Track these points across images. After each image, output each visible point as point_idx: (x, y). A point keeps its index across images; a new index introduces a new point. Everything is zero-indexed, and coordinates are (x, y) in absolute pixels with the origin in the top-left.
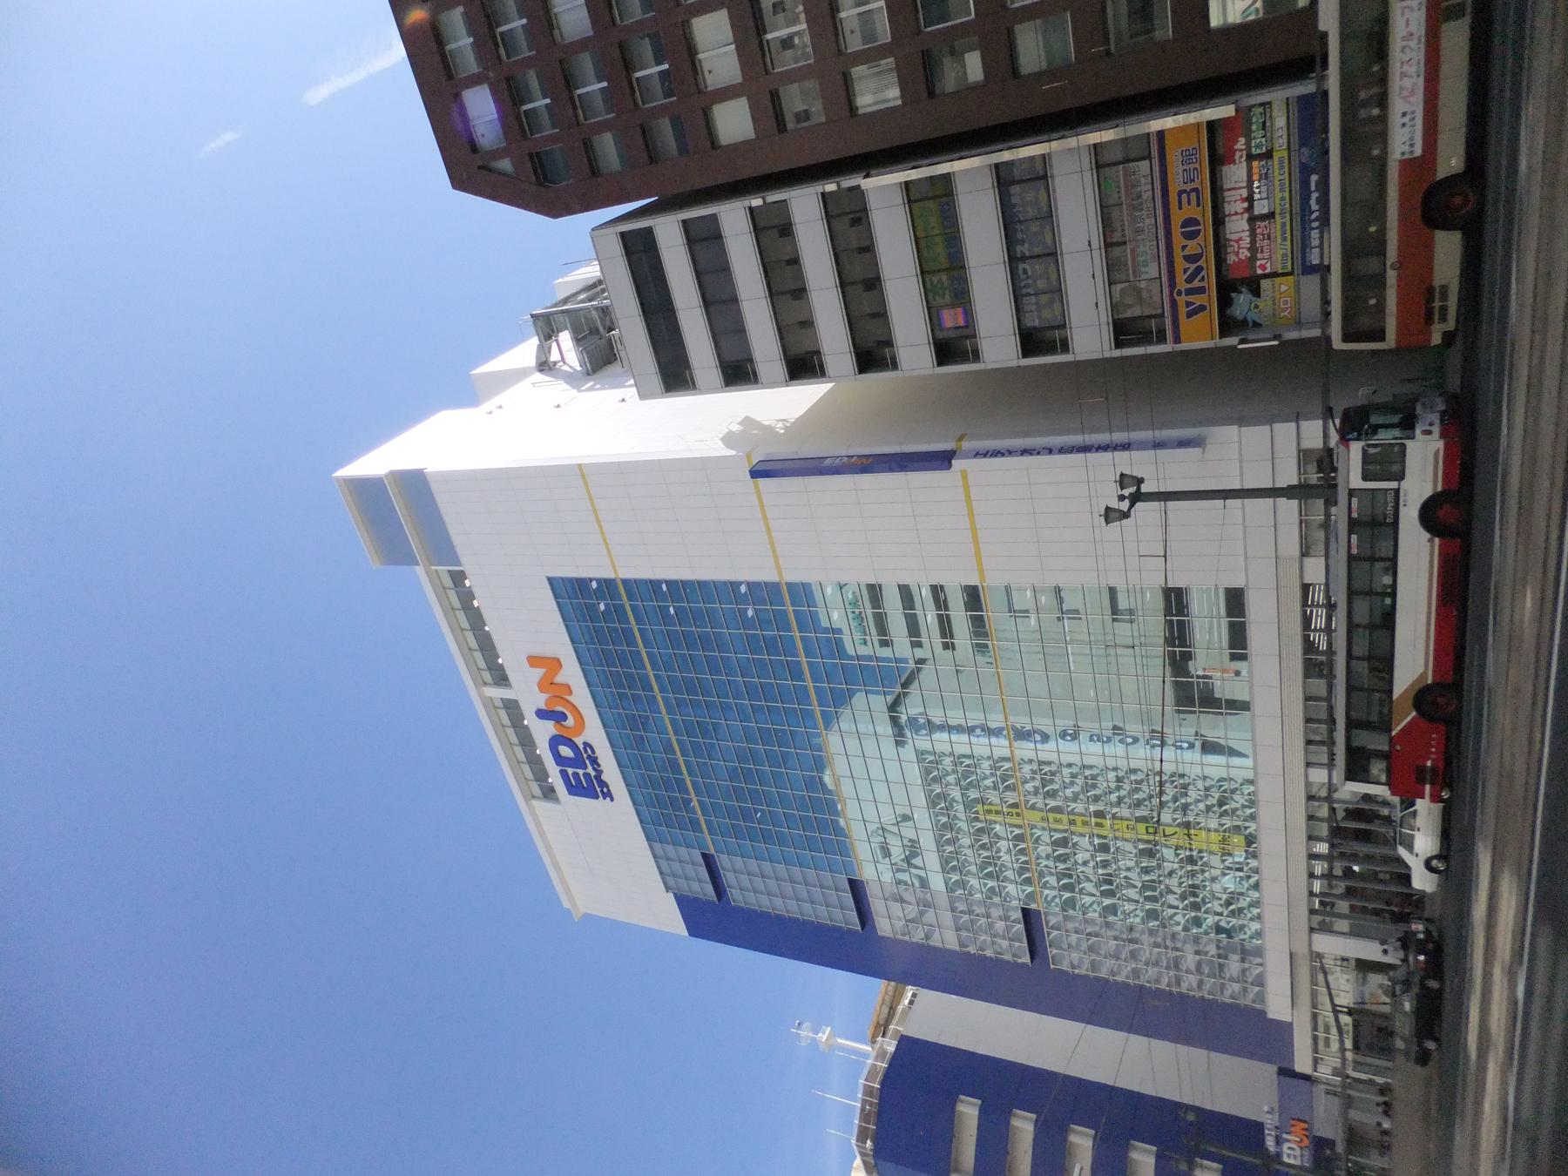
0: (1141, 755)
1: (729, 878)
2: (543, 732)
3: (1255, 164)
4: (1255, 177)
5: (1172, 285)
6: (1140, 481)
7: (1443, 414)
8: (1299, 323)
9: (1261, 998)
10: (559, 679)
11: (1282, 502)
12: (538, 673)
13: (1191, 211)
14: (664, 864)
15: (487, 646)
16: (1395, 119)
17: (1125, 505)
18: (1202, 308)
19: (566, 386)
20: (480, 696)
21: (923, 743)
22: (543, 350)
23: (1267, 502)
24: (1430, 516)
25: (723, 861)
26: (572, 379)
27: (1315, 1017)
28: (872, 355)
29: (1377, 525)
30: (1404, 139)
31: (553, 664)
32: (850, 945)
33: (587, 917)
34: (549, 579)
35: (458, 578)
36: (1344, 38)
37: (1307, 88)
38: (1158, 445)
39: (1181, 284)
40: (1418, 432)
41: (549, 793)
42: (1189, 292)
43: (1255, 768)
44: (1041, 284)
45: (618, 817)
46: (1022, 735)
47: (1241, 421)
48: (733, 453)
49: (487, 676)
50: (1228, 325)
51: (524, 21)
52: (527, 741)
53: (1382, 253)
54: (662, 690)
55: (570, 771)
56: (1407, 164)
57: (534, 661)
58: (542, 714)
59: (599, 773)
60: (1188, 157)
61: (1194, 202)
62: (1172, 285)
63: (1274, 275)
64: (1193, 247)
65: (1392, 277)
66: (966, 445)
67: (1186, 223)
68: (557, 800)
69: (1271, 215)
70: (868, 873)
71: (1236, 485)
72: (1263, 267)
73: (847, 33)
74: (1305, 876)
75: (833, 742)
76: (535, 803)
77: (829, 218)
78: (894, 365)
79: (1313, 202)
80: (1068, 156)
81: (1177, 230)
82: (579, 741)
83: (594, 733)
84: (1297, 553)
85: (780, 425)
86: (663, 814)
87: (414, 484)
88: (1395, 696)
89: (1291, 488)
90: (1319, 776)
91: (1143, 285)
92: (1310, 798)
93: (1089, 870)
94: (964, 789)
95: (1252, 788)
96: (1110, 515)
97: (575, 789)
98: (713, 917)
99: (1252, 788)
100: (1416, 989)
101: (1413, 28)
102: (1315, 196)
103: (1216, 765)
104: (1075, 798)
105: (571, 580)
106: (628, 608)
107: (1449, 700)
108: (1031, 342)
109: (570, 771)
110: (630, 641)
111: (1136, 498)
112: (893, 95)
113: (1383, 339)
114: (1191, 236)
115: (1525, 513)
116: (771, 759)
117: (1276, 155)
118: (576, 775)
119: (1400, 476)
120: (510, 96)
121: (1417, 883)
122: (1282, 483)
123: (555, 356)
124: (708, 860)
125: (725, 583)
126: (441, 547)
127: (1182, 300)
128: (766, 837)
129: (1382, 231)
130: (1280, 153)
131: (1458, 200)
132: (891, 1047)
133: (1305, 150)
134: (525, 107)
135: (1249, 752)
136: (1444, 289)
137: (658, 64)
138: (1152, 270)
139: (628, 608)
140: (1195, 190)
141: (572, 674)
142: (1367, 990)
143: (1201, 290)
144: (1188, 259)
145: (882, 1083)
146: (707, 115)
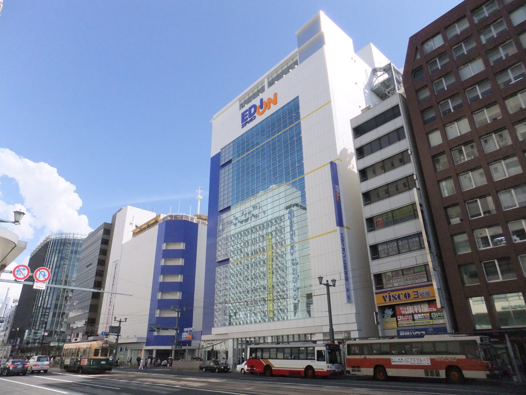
0: (291, 285)
1: (226, 168)
2: (256, 102)
3: (428, 314)
4: (425, 315)
5: (392, 291)
6: (334, 286)
7: (334, 371)
8: (384, 330)
9: (218, 326)
10: (272, 105)
11: (329, 327)
12: (272, 97)
13: (412, 296)
14: (224, 150)
15: (279, 77)
16: (400, 357)
17: (324, 282)
18: (385, 300)
19: (366, 82)
20: (264, 78)
21: (287, 217)
22: (380, 69)
23: (328, 323)
24: (309, 367)
25: (230, 166)
26: (370, 82)
27: (214, 340)
28: (368, 197)
29: (308, 354)
30: (396, 360)
31: (275, 103)
32: (216, 209)
33: (211, 124)
34: (298, 97)
35: (296, 63)
36: (421, 342)
37: (449, 329)
38: (348, 290)
39: (392, 294)
40: (329, 364)
41: (242, 106)
42: (390, 296)
43: (291, 320)
44: (390, 250)
45: (237, 130)
46: (292, 247)
47: (357, 314)
48: (338, 154)
49: (270, 79)
50: (383, 308)
51: (466, 53)
52: (255, 96)
53: (369, 354)
54: (278, 136)
55: (248, 113)
56: (389, 360)
57: (275, 95)
58: (262, 100)
59: (248, 122)
60: (428, 294)
61: (415, 296)
62: (392, 291)
63: (397, 321)
64: (402, 297)
65: (363, 357)
66: (345, 230)
67: (408, 293)
68: (240, 109)
69: (414, 320)
70: (233, 211)
71: (332, 314)
72: (399, 318)
73: (465, 176)
74: (311, 332)
75: (282, 188)
76: (238, 102)
77: (407, 177)
78: (365, 205)
79: (417, 332)
80: (425, 256)
81: (407, 291)
82: (256, 114)
83: (259, 119)
84: (324, 331)
85: (351, 166)
86: (241, 144)
87: (320, 42)
88: (269, 360)
89: (333, 330)
90: (269, 340)
91: (392, 281)
92: (264, 337)
93: (258, 271)
94: (275, 231)
95: (286, 319)
96: (321, 278)
97: (243, 115)
98: (217, 165)
99: (286, 319)
100: (215, 366)
101: (423, 362)
102: (419, 333)
103: (291, 308)
104: (277, 265)
105: (299, 104)
106: (293, 125)
107: (268, 373)
108: (374, 248)
109: (248, 113)
110: (252, 148)
111: (328, 285)
112: (446, 193)
113: (348, 355)
114: (405, 297)
115: (275, 389)
116: (258, 178)
117: (431, 321)
118: (247, 115)
119: (318, 360)
120: (440, 53)
121: (238, 366)
122: (334, 327)
123: (379, 74)
124: (230, 161)
125: (302, 156)
126: (305, 55)
127: (387, 294)
128: (238, 179)
129: (375, 354)
130: (431, 322)
131: (381, 374)
132: (195, 221)
133: (432, 330)
134: (437, 60)
135: (296, 317)
136: (360, 371)
137: (453, 108)
138: (396, 285)
139: (293, 125)
140: (418, 296)
141: (274, 109)
142: (222, 354)
143: (390, 300)
144: (399, 295)
145: (185, 221)
146: (436, 129)
